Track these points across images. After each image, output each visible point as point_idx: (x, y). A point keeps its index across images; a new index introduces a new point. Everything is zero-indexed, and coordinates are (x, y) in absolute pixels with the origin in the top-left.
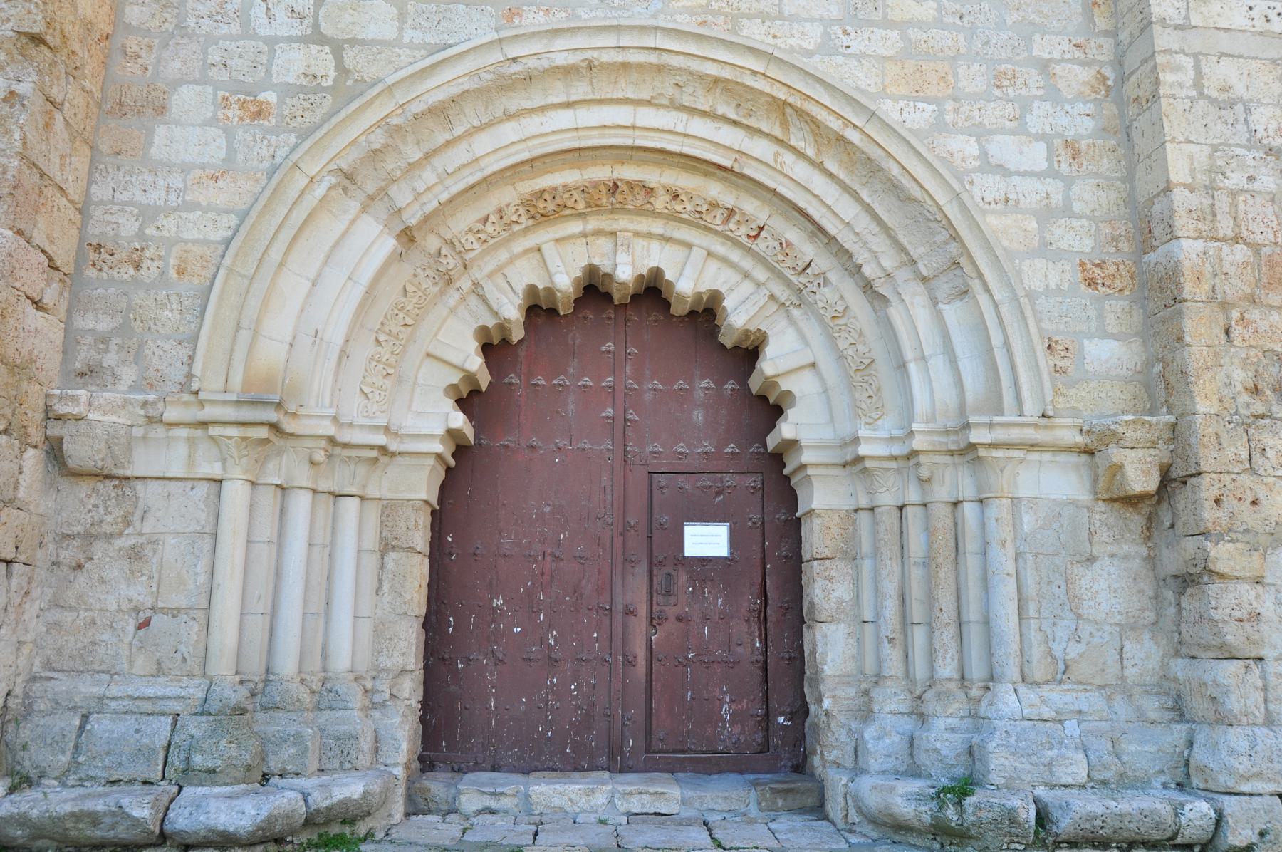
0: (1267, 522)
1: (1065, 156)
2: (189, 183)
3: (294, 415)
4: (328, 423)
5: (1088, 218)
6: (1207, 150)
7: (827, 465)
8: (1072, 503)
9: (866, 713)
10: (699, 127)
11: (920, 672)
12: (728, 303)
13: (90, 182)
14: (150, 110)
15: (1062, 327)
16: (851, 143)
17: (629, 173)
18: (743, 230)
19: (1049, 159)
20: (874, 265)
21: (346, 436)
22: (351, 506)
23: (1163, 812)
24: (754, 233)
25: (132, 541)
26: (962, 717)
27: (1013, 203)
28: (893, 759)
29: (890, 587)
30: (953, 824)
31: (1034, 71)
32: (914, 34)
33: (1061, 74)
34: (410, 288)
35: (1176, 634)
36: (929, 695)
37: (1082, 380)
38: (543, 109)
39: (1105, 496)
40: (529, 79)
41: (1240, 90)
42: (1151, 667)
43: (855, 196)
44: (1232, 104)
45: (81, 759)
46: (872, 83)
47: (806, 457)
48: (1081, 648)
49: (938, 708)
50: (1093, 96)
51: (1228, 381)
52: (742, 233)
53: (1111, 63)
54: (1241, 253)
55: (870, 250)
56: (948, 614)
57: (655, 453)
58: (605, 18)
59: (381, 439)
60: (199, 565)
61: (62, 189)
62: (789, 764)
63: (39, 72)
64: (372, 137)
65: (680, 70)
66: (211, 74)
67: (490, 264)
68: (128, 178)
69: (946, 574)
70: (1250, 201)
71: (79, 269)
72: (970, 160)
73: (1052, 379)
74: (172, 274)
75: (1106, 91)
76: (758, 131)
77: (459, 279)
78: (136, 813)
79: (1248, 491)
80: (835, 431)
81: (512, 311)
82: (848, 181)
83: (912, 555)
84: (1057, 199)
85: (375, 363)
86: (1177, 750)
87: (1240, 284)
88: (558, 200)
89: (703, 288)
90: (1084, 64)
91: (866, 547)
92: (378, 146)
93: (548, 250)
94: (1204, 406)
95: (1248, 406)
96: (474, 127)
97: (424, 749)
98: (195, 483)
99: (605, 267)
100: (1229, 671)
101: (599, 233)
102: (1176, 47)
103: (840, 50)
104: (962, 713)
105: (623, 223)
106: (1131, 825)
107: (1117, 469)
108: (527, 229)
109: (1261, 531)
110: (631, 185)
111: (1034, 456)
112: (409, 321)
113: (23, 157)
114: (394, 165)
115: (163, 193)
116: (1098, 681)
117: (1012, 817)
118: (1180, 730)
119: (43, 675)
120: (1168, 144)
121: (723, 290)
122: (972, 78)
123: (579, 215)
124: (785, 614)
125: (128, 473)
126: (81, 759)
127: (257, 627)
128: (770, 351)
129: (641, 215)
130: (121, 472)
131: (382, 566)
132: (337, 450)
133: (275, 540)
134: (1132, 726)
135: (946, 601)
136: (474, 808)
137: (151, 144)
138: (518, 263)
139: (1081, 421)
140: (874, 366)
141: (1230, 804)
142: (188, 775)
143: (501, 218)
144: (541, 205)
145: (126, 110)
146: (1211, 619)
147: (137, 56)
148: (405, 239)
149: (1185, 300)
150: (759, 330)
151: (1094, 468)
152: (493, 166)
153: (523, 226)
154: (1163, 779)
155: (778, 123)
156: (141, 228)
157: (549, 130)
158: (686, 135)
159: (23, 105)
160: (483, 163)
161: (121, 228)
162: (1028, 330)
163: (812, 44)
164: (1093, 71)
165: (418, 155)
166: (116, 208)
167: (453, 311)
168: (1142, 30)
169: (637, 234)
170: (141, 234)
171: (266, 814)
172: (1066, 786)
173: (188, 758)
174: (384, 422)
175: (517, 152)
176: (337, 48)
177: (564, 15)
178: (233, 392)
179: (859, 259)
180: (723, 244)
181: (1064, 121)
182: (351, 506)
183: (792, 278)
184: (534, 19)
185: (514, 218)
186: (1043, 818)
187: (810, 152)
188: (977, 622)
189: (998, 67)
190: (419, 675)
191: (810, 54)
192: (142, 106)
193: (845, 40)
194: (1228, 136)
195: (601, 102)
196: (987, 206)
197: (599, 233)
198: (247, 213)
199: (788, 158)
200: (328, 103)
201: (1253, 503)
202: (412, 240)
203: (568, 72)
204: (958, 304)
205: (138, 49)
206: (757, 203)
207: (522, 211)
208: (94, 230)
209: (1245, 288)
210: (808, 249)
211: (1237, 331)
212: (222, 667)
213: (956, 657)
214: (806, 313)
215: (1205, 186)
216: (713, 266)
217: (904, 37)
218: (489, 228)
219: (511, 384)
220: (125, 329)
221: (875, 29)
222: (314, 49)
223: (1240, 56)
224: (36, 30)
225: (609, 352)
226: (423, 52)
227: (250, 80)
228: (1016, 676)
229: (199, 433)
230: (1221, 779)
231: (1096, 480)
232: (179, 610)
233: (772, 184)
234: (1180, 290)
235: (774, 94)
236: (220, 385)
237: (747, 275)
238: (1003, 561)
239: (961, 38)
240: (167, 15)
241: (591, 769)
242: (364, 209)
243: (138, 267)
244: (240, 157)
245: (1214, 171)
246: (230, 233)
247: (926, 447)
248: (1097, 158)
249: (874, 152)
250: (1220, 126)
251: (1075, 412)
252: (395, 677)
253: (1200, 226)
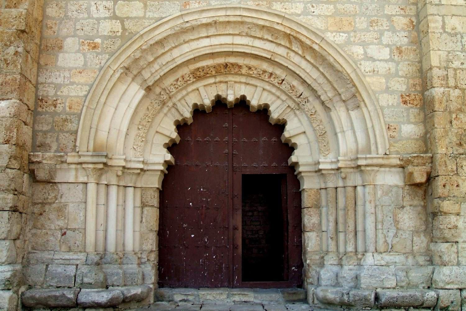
0: (462, 193)
1: (397, 54)
2: (71, 75)
3: (111, 159)
4: (123, 161)
5: (405, 78)
6: (446, 53)
7: (309, 172)
8: (397, 186)
9: (322, 265)
10: (258, 43)
11: (342, 250)
12: (271, 109)
14: (57, 48)
15: (393, 120)
16: (315, 49)
17: (232, 60)
18: (276, 80)
20: (325, 95)
21: (129, 165)
22: (130, 191)
23: (418, 295)
24: (280, 82)
26: (355, 266)
27: (376, 72)
28: (330, 281)
29: (332, 219)
30: (346, 301)
31: (385, 20)
33: (396, 20)
34: (150, 108)
35: (432, 234)
36: (344, 258)
37: (400, 140)
38: (198, 39)
39: (409, 183)
40: (193, 28)
41: (459, 29)
42: (423, 246)
43: (317, 69)
44: (456, 34)
45: (48, 279)
46: (323, 26)
47: (301, 169)
49: (346, 262)
50: (408, 29)
51: (450, 141)
52: (276, 82)
53: (415, 16)
54: (457, 92)
55: (324, 90)
56: (351, 228)
57: (245, 167)
59: (141, 166)
60: (81, 213)
61: (30, 81)
62: (296, 285)
63: (24, 42)
64: (136, 54)
65: (249, 23)
66: (77, 33)
67: (179, 96)
68: (50, 74)
70: (462, 73)
71: (36, 109)
72: (360, 55)
73: (389, 140)
75: (413, 27)
76: (280, 44)
77: (167, 102)
78: (69, 296)
79: (455, 182)
80: (312, 159)
81: (187, 114)
82: (315, 64)
83: (339, 206)
84: (393, 70)
85: (138, 137)
86: (429, 275)
87: (456, 104)
88: (205, 71)
89: (262, 103)
90: (404, 16)
91: (324, 203)
92: (137, 57)
93: (202, 90)
95: (457, 151)
96: (173, 47)
97: (160, 280)
98: (78, 184)
99: (224, 96)
100: (444, 247)
101: (221, 82)
102: (435, 13)
103: (311, 13)
104: (355, 264)
105: (230, 78)
106: (407, 300)
107: (411, 174)
108: (193, 82)
109: (459, 196)
110: (233, 65)
111: (382, 169)
112: (150, 120)
113: (21, 74)
114: (144, 63)
115: (63, 79)
116: (403, 251)
117: (366, 299)
118: (430, 268)
119: (32, 251)
120: (431, 51)
121: (269, 103)
122: (361, 23)
123: (213, 76)
124: (295, 229)
125: (56, 181)
126: (48, 279)
127: (101, 234)
129: (237, 75)
130: (53, 181)
131: (142, 212)
132: (126, 170)
133: (105, 204)
134: (414, 267)
136: (179, 300)
137: (58, 61)
138: (190, 95)
139: (399, 156)
140: (326, 134)
142: (83, 285)
143: (183, 79)
144: (198, 73)
145: (48, 48)
146: (440, 228)
147: (52, 28)
148: (148, 89)
149: (435, 111)
150: (283, 119)
151: (404, 172)
152: (179, 61)
153: (192, 81)
155: (288, 42)
156: (56, 92)
157: (201, 46)
158: (253, 47)
159: (20, 56)
160: (176, 60)
161: (49, 92)
162: (380, 122)
163: (300, 11)
164: (408, 19)
165: (152, 59)
166: (47, 85)
167: (166, 115)
168: (424, 5)
169: (235, 82)
170: (56, 94)
171: (111, 297)
172: (388, 288)
173: (82, 280)
174: (141, 159)
175: (189, 55)
177: (205, 4)
178: (90, 151)
179: (319, 93)
180: (269, 85)
181: (396, 39)
182: (130, 191)
183: (295, 99)
184: (195, 6)
185: (188, 79)
186: (377, 298)
187: (300, 52)
188: (361, 231)
189: (372, 18)
191: (299, 15)
192: (54, 47)
193: (312, 10)
194: (454, 47)
195: (220, 35)
196: (366, 74)
197: (221, 82)
198: (92, 85)
199: (292, 54)
201: (457, 186)
202: (150, 89)
203: (207, 25)
204: (356, 111)
205: (51, 25)
206: (281, 70)
207: (191, 76)
209: (458, 106)
210: (301, 88)
211: (454, 122)
212: (90, 248)
213: (354, 244)
214: (301, 112)
215: (445, 67)
216: (265, 94)
217: (335, 7)
218: (179, 83)
219: (188, 141)
221: (324, 5)
222: (114, 21)
223: (460, 16)
224: (23, 28)
225: (226, 127)
226: (154, 21)
227: (91, 34)
228: (374, 250)
229: (79, 166)
230: (440, 284)
231: (405, 178)
232: (75, 229)
233: (286, 65)
234: (434, 107)
235: (286, 31)
236: (86, 149)
237: (278, 97)
238: (370, 208)
239: (357, 7)
240: (61, 11)
241: (221, 287)
242: (133, 80)
243: (55, 107)
244: (89, 64)
245: (448, 61)
246: (86, 93)
247: (343, 166)
248: (408, 54)
249: (324, 53)
251: (398, 153)
252: (149, 253)
253: (442, 83)
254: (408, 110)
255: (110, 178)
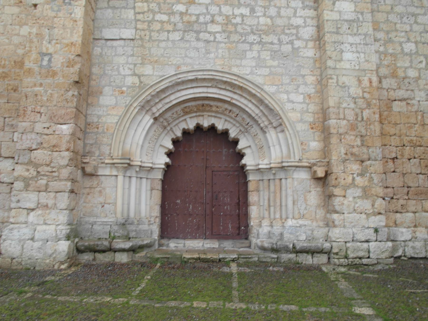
1: (307, 98)
9: (260, 226)
10: (222, 92)
13: (87, 110)
19: (304, 99)
21: (143, 165)
25: (100, 189)
29: (266, 198)
32: (273, 69)
34: (157, 130)
36: (274, 222)
41: (347, 83)
43: (259, 108)
44: (345, 87)
47: (248, 168)
48: (307, 211)
52: (233, 115)
54: (345, 122)
56: (278, 204)
58: (200, 68)
59: (150, 165)
64: (148, 98)
67: (174, 123)
69: (278, 195)
73: (302, 152)
74: (105, 130)
84: (305, 109)
89: (224, 128)
90: (313, 75)
94: (334, 158)
116: (310, 218)
118: (327, 229)
122: (286, 80)
127: (126, 206)
128: (240, 143)
132: (142, 168)
135: (278, 201)
141: (334, 244)
154: (323, 239)
174: (151, 161)
176: (139, 76)
182: (144, 180)
190: (160, 217)
193: (256, 71)
200: (138, 90)
208: (88, 120)
210: (248, 120)
211: (343, 140)
212: (119, 215)
216: (227, 123)
217: (270, 70)
220: (96, 143)
222: (134, 77)
223: (348, 75)
229: (112, 165)
238: (290, 192)
245: (340, 103)
250: (342, 92)
254: (314, 133)
255: (131, 173)
